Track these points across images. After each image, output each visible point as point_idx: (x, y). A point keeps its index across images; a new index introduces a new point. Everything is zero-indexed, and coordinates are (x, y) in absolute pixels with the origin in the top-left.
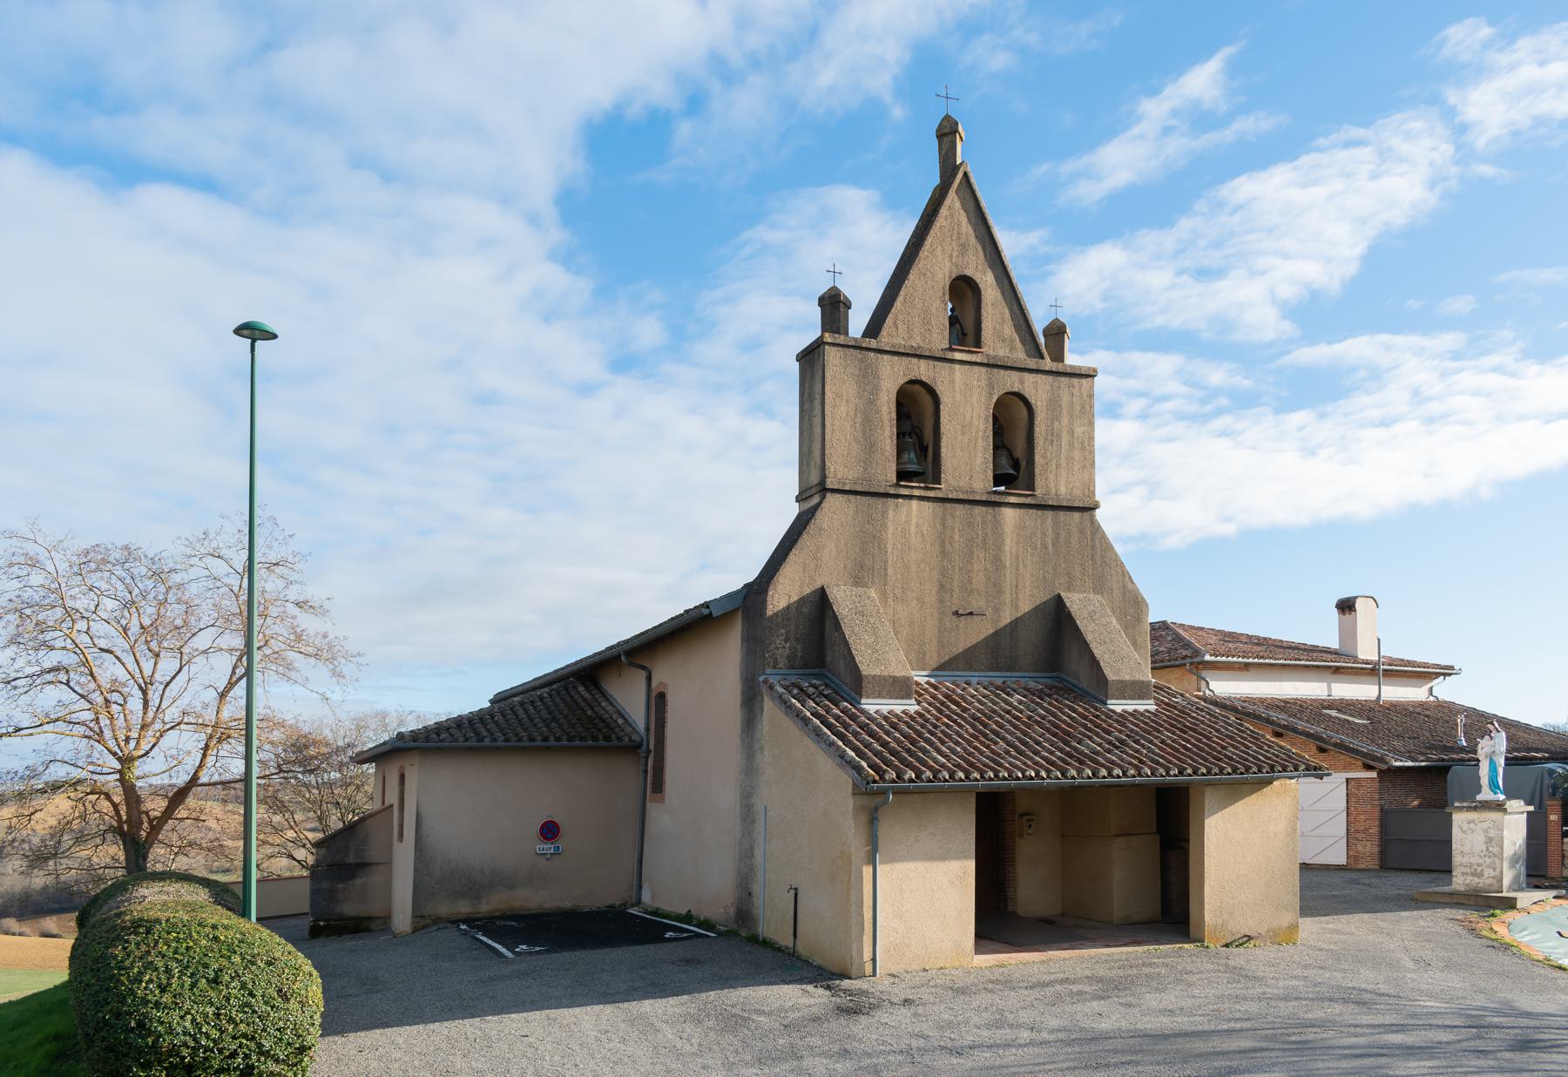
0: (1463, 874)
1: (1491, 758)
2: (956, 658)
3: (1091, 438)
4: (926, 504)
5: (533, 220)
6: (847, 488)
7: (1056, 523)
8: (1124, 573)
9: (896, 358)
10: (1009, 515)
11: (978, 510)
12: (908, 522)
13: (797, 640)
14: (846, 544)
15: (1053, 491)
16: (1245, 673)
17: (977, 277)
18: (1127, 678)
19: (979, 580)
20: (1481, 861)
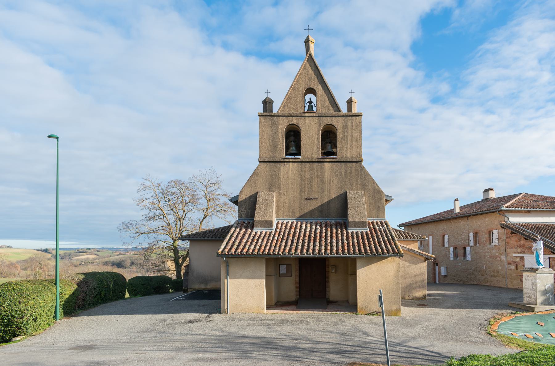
0: (527, 297)
1: (536, 251)
2: (306, 214)
3: (360, 137)
4: (295, 164)
5: (404, 55)
6: (266, 160)
7: (345, 167)
8: (374, 183)
9: (284, 118)
10: (327, 166)
11: (315, 165)
12: (288, 170)
13: (249, 209)
14: (266, 179)
15: (345, 156)
16: (529, 214)
17: (315, 88)
18: (357, 220)
19: (315, 188)
20: (531, 292)
